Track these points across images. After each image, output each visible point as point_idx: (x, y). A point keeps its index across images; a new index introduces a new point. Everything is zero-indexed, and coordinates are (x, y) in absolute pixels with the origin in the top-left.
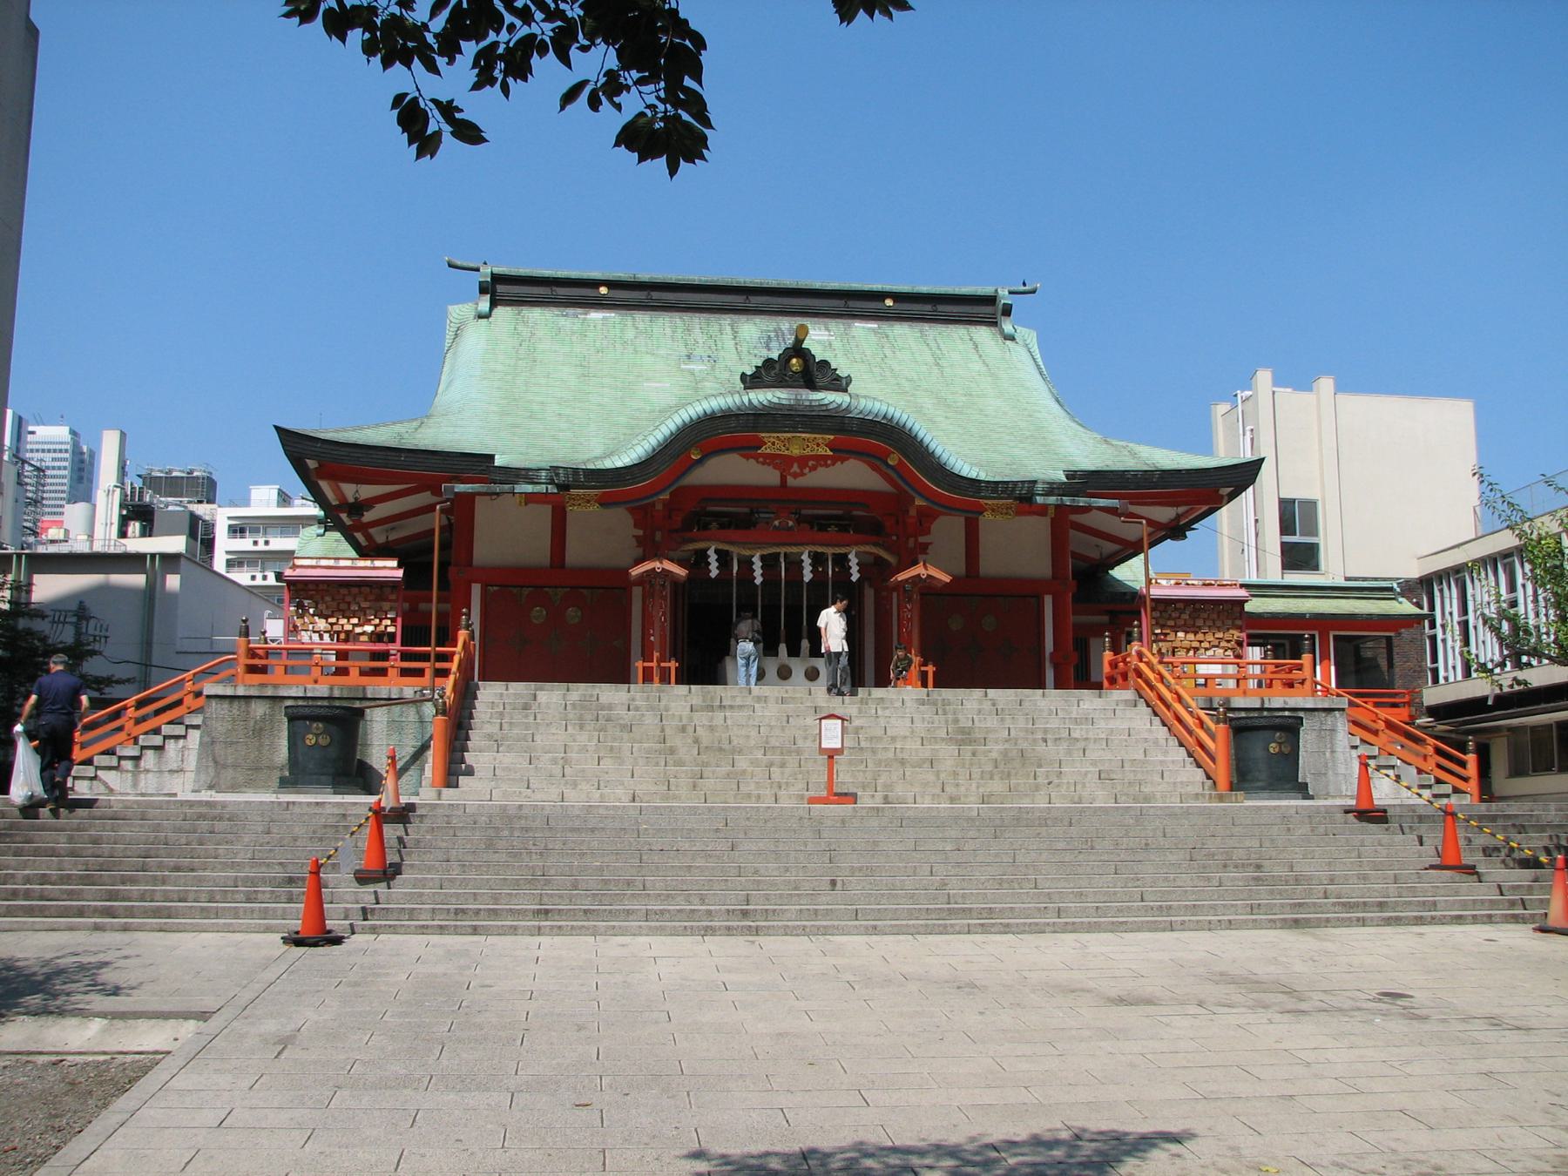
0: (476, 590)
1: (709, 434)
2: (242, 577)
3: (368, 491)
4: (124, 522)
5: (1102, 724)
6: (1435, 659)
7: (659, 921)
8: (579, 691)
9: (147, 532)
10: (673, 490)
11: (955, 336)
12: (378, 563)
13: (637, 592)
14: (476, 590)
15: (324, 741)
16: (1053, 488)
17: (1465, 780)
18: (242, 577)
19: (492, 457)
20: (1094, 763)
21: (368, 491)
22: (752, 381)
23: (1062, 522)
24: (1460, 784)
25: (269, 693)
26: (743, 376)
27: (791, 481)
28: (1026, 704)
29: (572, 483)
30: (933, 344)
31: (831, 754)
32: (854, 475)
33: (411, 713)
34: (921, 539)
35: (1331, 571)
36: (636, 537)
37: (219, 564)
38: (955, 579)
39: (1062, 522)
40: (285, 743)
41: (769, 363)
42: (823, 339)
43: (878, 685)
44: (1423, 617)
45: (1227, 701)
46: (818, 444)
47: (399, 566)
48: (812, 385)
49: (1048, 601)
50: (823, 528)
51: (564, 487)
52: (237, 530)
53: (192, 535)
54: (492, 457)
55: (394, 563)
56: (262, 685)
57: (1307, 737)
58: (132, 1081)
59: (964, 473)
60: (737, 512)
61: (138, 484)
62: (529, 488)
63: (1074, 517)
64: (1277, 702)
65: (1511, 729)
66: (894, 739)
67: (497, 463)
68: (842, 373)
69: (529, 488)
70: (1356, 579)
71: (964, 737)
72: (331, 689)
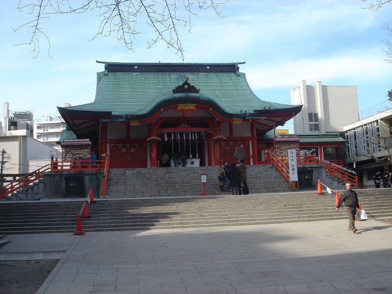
0: (108, 145)
1: (165, 104)
2: (41, 140)
4: (10, 126)
6: (349, 152)
8: (136, 170)
9: (16, 129)
12: (84, 140)
13: (148, 144)
14: (108, 145)
15: (74, 185)
16: (251, 115)
18: (41, 140)
19: (111, 112)
23: (253, 123)
31: (204, 183)
32: (201, 114)
35: (323, 131)
36: (175, 164)
37: (35, 137)
38: (227, 138)
39: (253, 123)
40: (64, 185)
42: (193, 79)
44: (345, 142)
48: (190, 92)
49: (251, 142)
51: (130, 119)
52: (39, 128)
53: (28, 129)
54: (111, 112)
55: (89, 140)
57: (315, 174)
58: (53, 267)
59: (229, 112)
60: (174, 123)
61: (13, 116)
62: (121, 120)
63: (257, 121)
64: (307, 166)
65: (368, 169)
66: (213, 179)
70: (328, 133)
72: (75, 172)
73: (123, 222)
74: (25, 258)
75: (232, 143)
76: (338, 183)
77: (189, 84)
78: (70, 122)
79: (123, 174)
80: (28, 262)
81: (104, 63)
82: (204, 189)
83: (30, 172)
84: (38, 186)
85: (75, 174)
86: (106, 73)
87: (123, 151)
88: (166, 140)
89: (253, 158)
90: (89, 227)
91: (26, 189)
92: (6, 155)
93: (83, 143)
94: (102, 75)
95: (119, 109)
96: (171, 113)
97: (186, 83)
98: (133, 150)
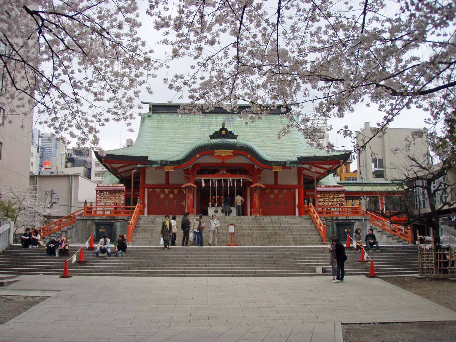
1: (201, 150)
3: (117, 166)
5: (299, 225)
7: (163, 274)
10: (196, 163)
11: (276, 118)
14: (146, 190)
17: (408, 237)
19: (147, 158)
20: (293, 235)
21: (117, 166)
22: (212, 137)
24: (406, 239)
25: (92, 218)
26: (210, 136)
27: (224, 162)
28: (280, 220)
29: (164, 164)
30: (270, 121)
31: (232, 234)
32: (240, 160)
33: (417, 185)
34: (259, 176)
40: (95, 230)
41: (216, 132)
43: (243, 215)
45: (337, 218)
46: (230, 153)
47: (124, 186)
49: (297, 190)
50: (235, 173)
54: (147, 158)
56: (90, 216)
62: (156, 166)
66: (243, 229)
67: (149, 159)
68: (235, 134)
69: (156, 166)
71: (262, 228)
73: (129, 269)
74: (24, 294)
75: (276, 191)
76: (388, 237)
77: (226, 130)
78: (109, 167)
79: (153, 222)
80: (25, 297)
81: (148, 103)
82: (232, 239)
83: (441, 161)
84: (71, 230)
85: (107, 220)
86: (151, 114)
87: (161, 197)
88: (203, 186)
89: (299, 208)
90: (96, 272)
91: (60, 233)
92: (55, 196)
93: (118, 188)
94: (146, 116)
95: (155, 154)
96: (207, 160)
97: (223, 129)
98: (171, 196)
